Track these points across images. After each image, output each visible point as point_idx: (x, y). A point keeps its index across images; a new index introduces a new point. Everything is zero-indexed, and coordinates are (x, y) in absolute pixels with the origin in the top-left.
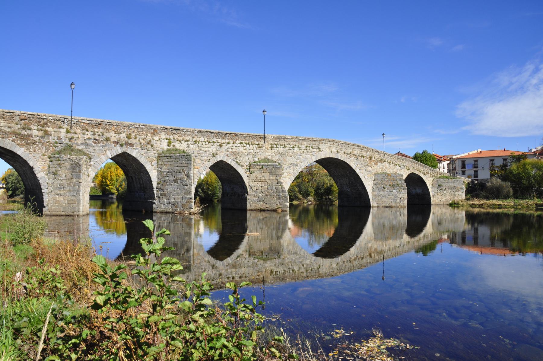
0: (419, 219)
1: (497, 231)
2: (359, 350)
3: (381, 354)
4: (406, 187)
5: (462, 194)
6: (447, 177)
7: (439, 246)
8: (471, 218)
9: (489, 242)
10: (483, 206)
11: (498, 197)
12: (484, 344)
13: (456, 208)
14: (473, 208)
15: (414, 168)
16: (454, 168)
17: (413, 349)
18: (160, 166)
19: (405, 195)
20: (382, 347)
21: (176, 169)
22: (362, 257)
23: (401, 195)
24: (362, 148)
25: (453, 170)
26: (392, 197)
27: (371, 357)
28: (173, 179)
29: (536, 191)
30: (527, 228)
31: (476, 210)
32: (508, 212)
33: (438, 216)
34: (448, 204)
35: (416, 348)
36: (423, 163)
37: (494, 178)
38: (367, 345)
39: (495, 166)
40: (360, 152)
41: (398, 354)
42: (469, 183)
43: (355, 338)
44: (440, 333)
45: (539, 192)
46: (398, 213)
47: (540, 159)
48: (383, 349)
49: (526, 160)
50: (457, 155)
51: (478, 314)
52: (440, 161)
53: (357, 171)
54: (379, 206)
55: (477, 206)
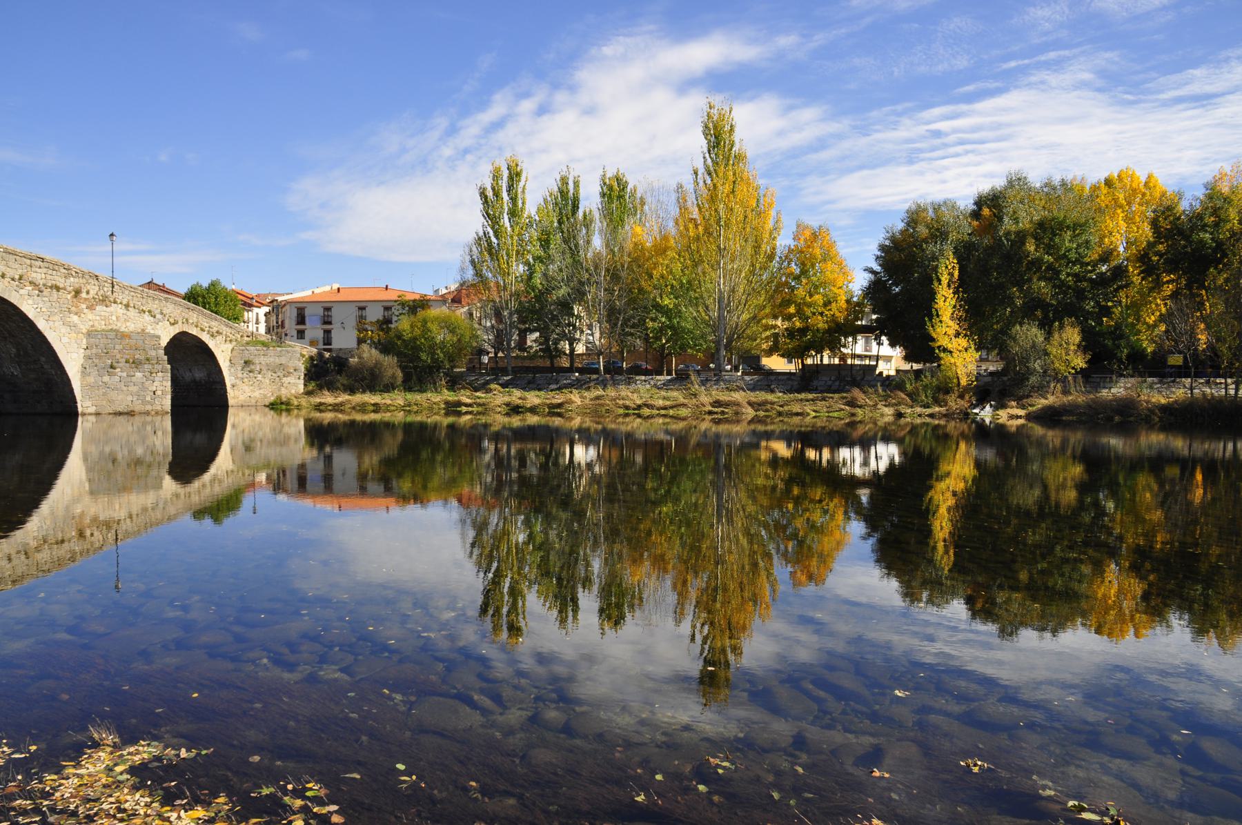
0: (200, 439)
1: (371, 460)
2: (55, 789)
3: (118, 787)
4: (169, 366)
5: (298, 381)
6: (264, 344)
7: (247, 501)
8: (318, 434)
9: (354, 484)
10: (342, 408)
11: (372, 388)
12: (352, 713)
13: (284, 414)
14: (321, 411)
15: (187, 320)
16: (280, 323)
17: (195, 757)
19: (165, 383)
20: (119, 769)
22: (60, 539)
23: (155, 384)
24: (53, 266)
25: (278, 327)
26: (134, 389)
27: (89, 800)
29: (446, 374)
30: (429, 451)
31: (328, 417)
32: (392, 419)
33: (243, 431)
34: (267, 404)
35: (204, 752)
36: (209, 309)
37: (365, 347)
38: (78, 772)
39: (367, 321)
40: (49, 277)
41: (161, 778)
42: (311, 358)
43: (41, 761)
44: (258, 705)
45: (451, 377)
46: (149, 428)
47: (454, 311)
48: (121, 773)
49: (429, 311)
50: (287, 294)
51: (337, 649)
52: (249, 306)
53: (41, 325)
54: (100, 411)
55: (330, 408)
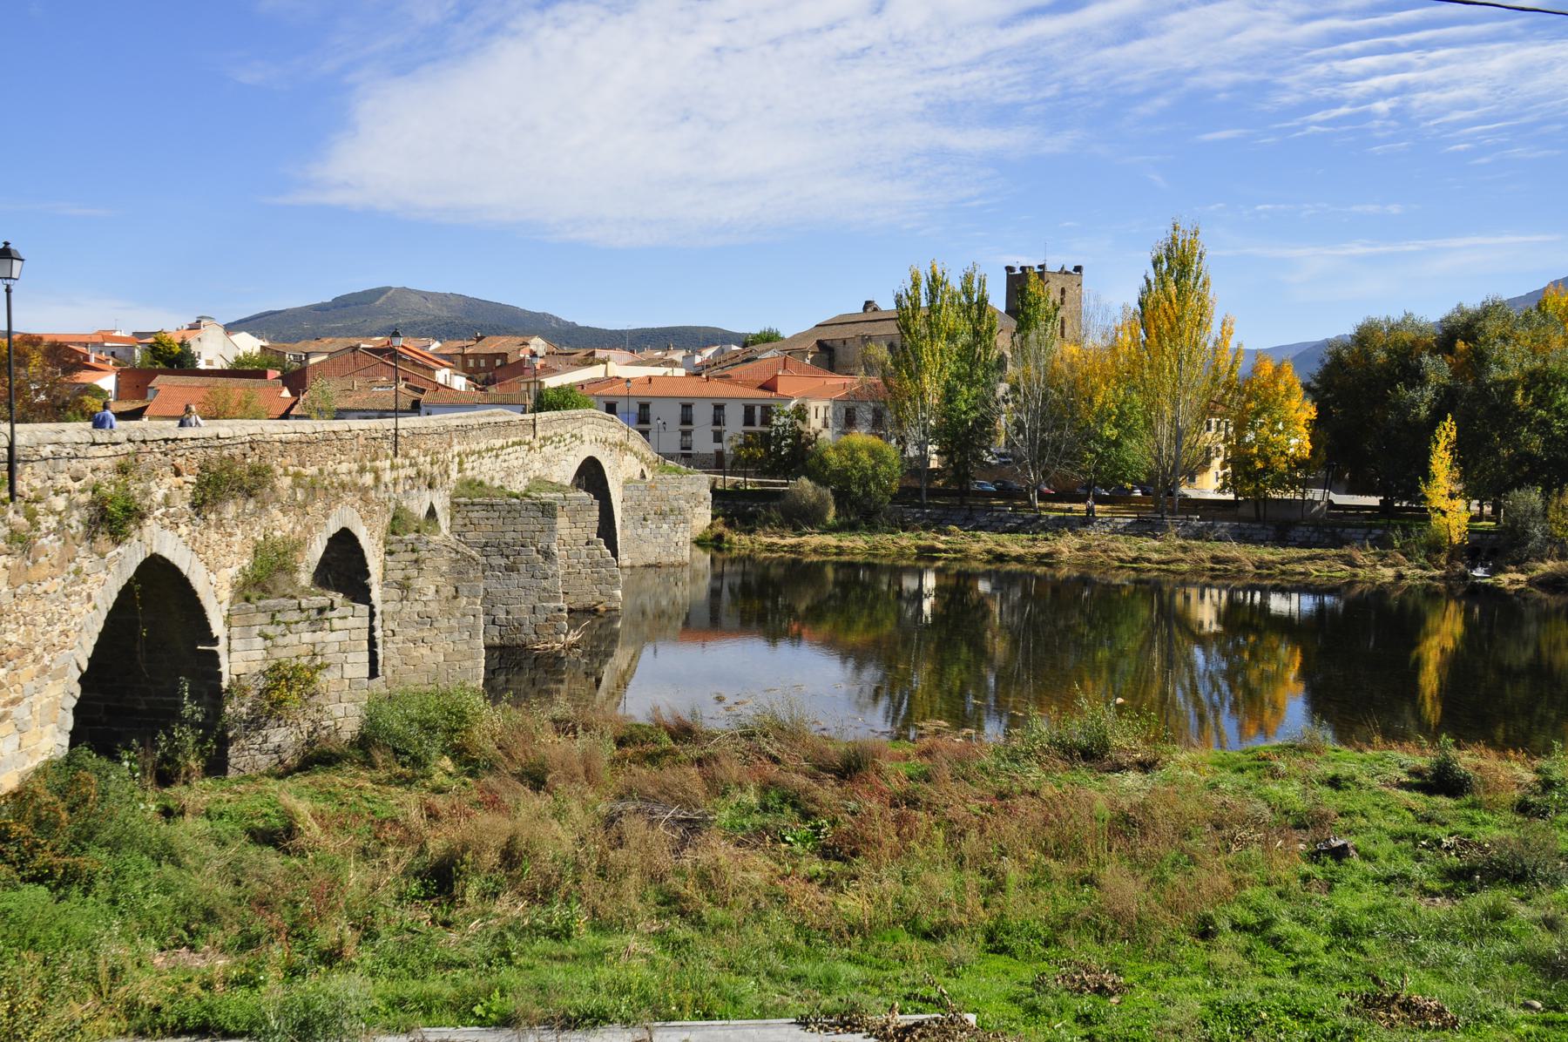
18: (459, 528)
21: (509, 537)
26: (661, 540)
28: (503, 562)
